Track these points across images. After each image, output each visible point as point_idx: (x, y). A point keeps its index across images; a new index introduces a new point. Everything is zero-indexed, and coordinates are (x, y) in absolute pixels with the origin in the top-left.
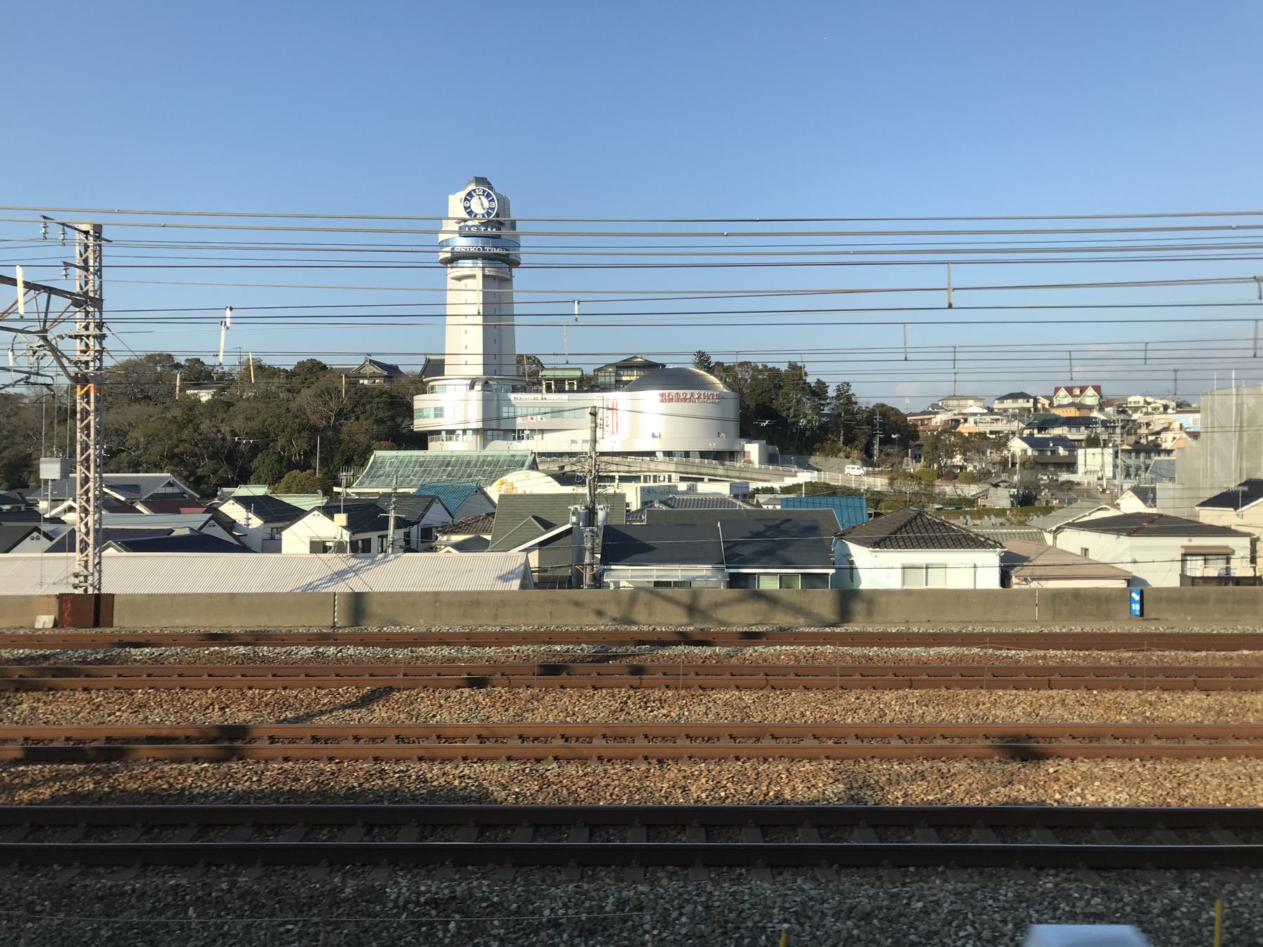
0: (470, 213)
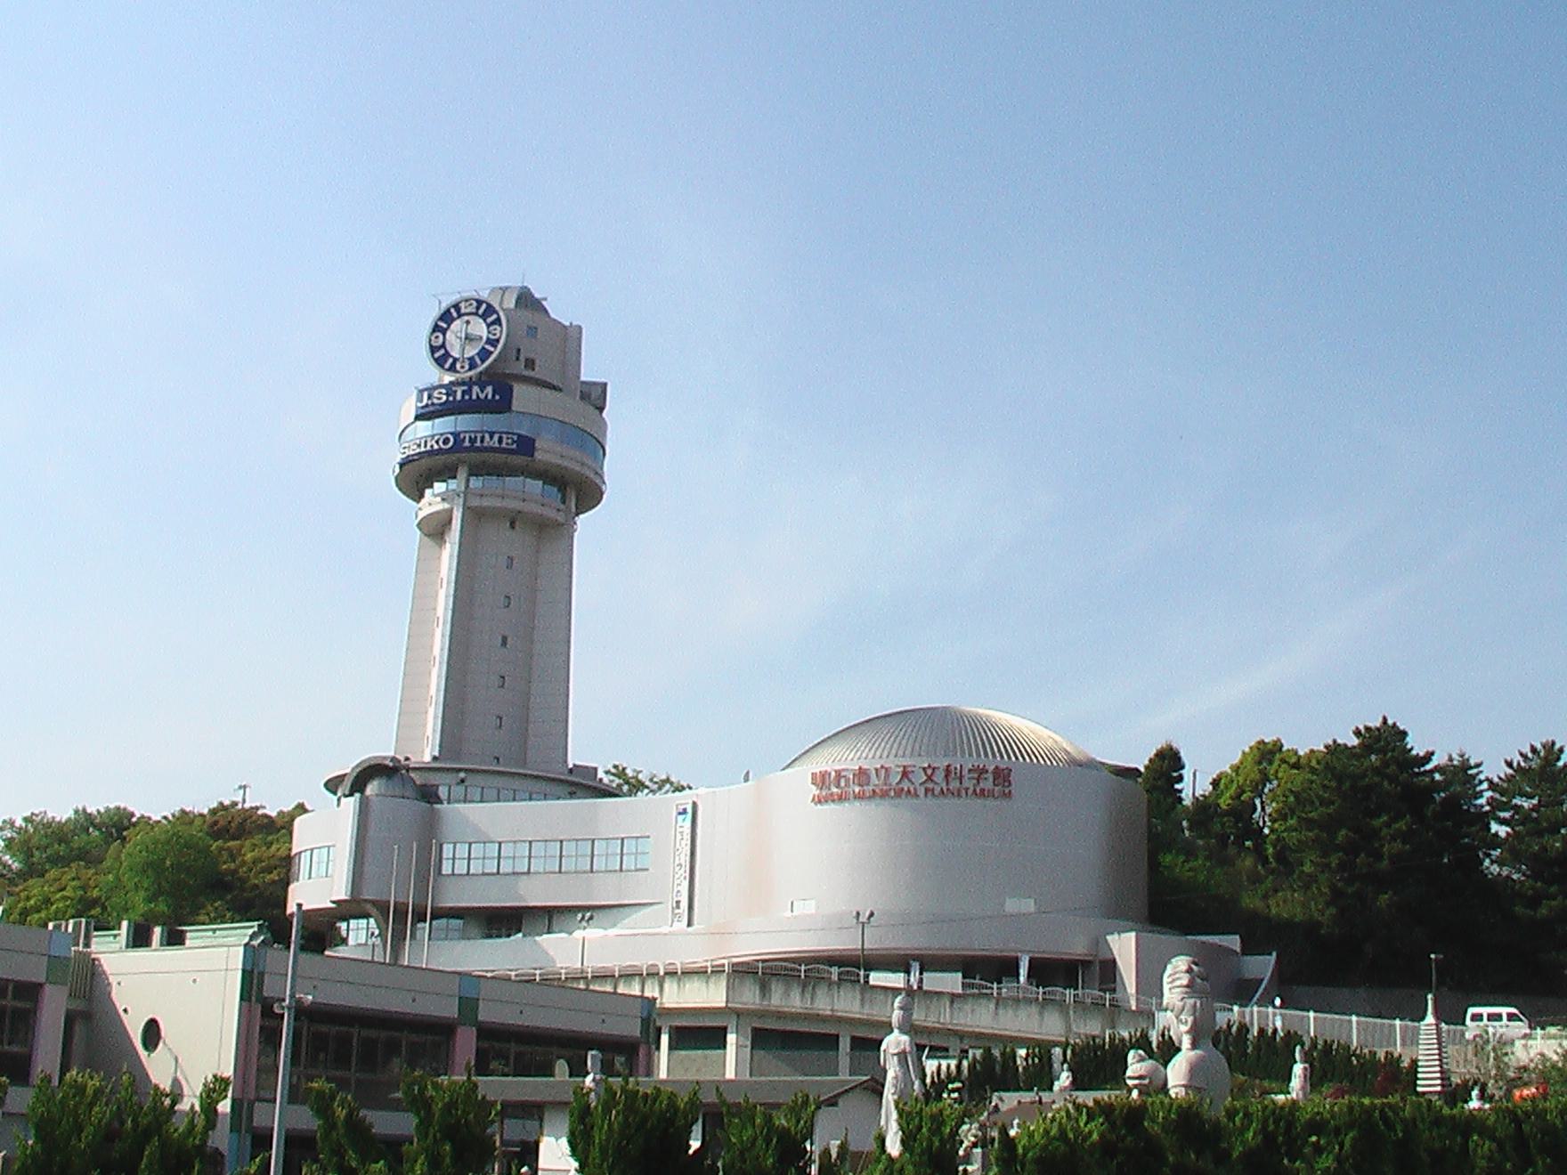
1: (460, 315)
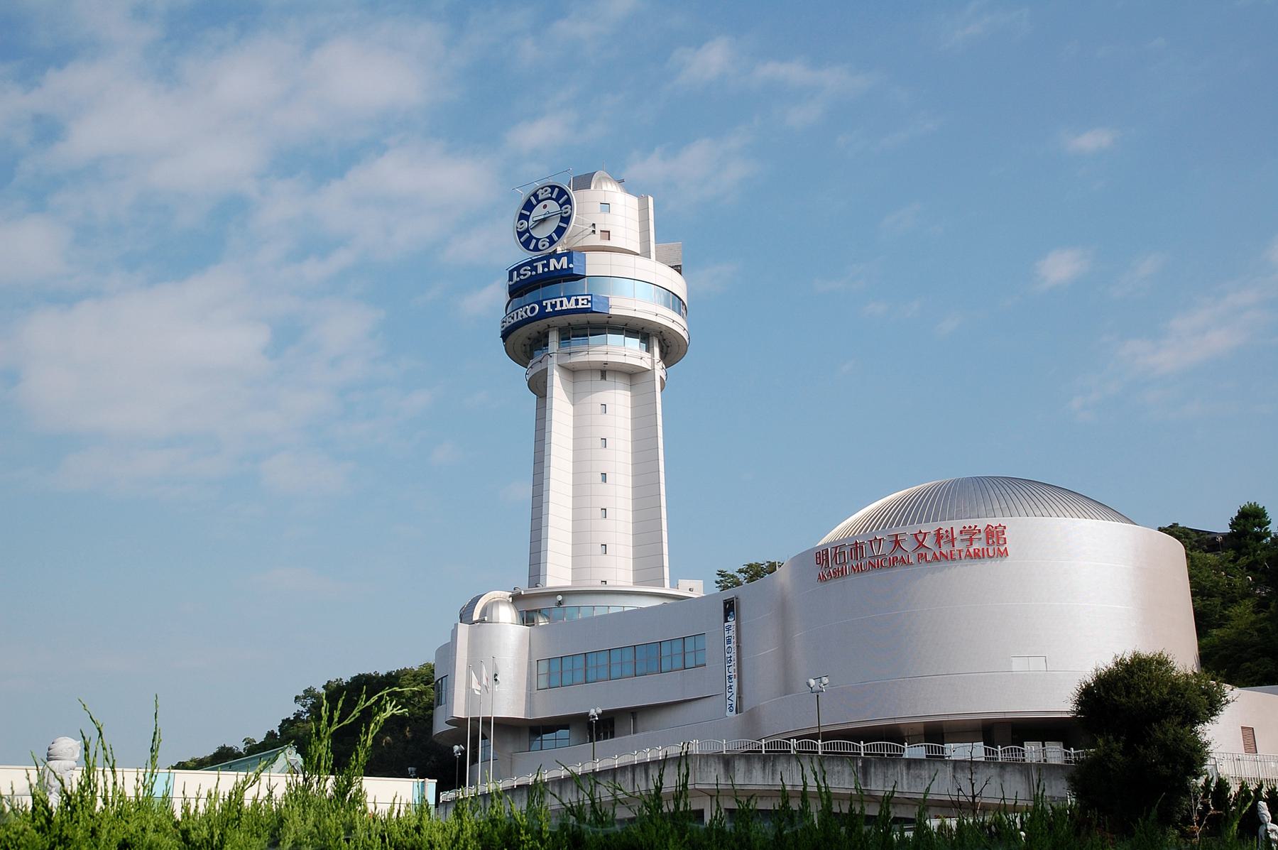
1: (539, 202)
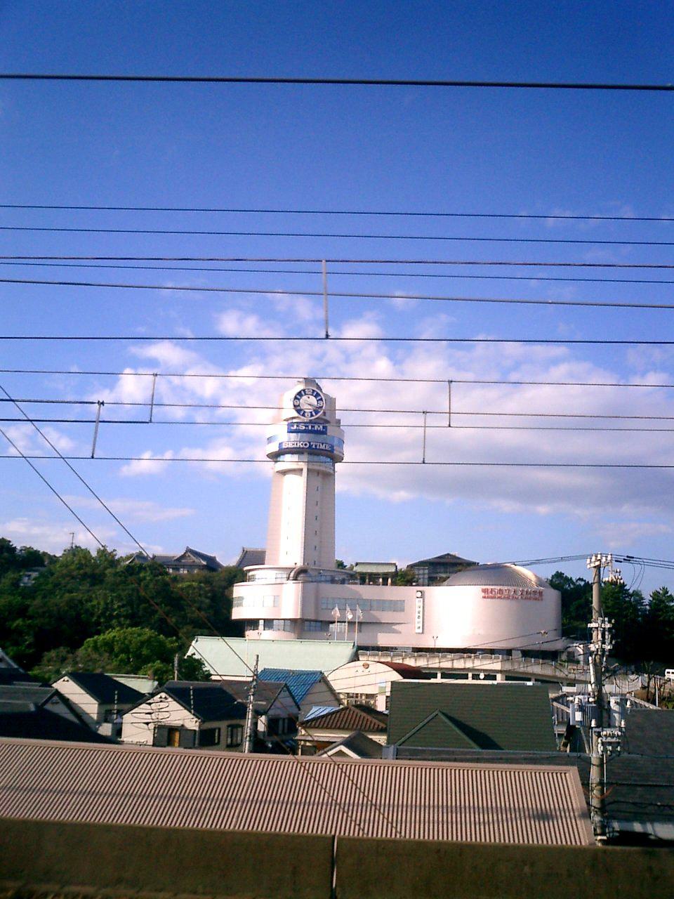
0: (299, 411)
1: (305, 394)
